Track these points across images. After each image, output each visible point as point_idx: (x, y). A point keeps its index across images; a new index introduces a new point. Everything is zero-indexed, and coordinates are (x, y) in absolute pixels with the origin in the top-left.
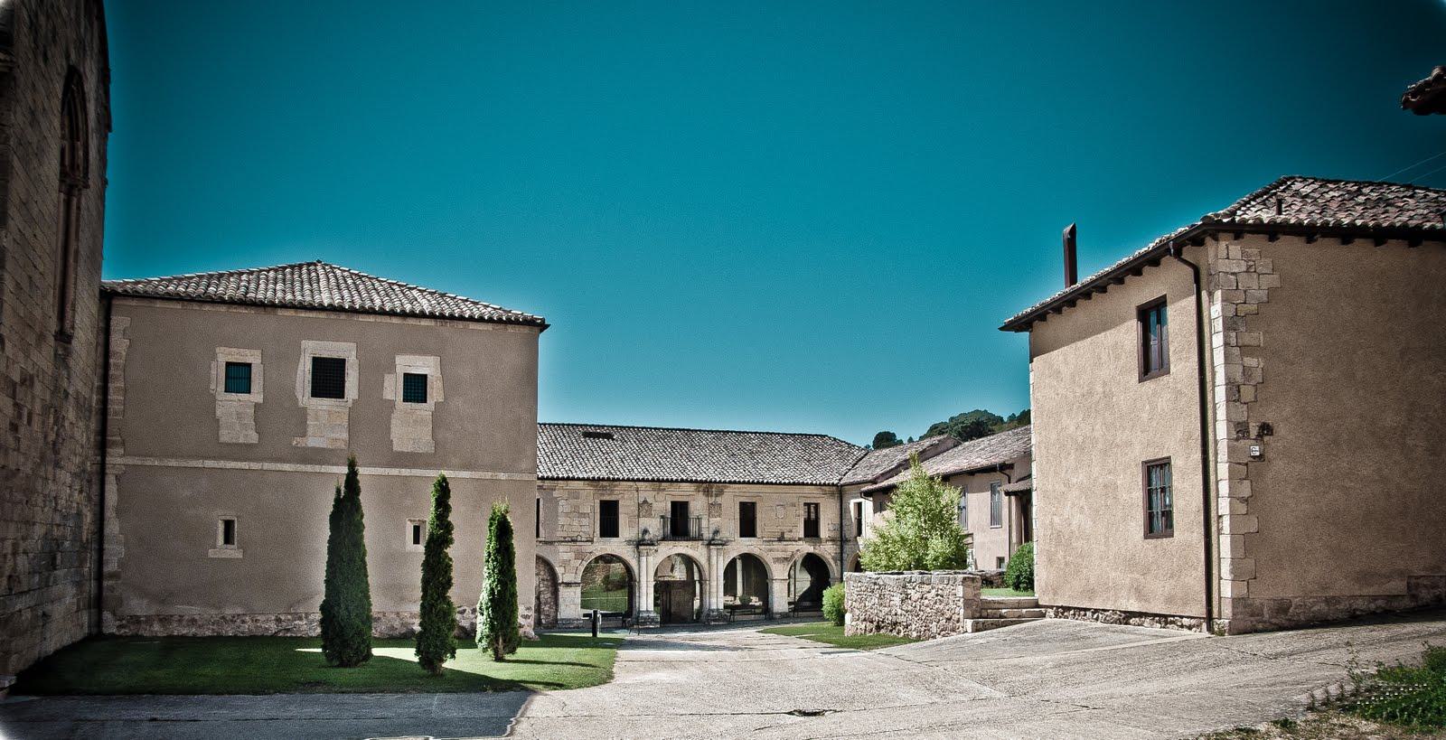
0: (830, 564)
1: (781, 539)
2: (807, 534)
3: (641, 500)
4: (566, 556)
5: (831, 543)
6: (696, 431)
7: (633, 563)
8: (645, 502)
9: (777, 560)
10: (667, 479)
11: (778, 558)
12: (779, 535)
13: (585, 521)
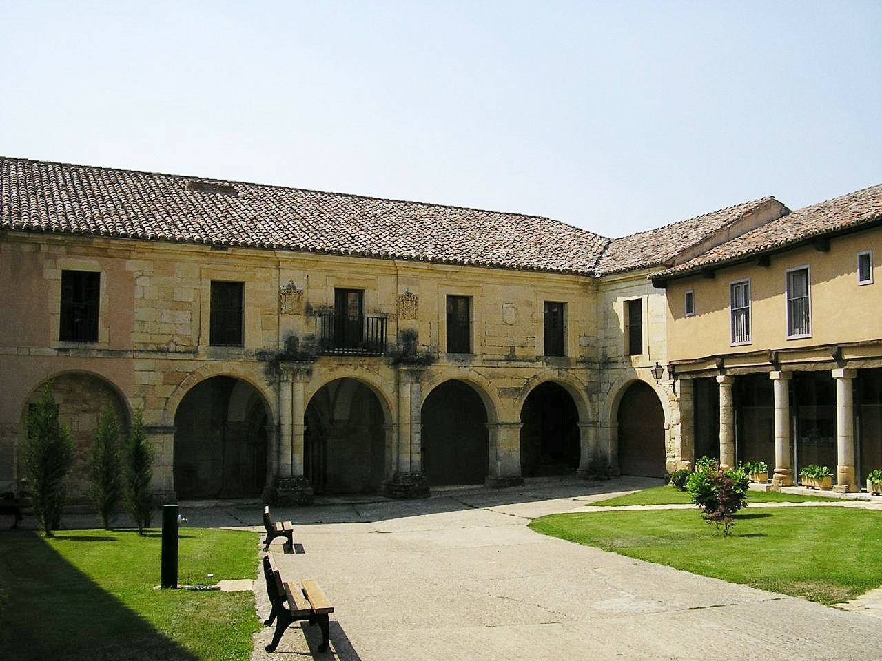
0: (581, 399)
1: (510, 358)
2: (548, 351)
3: (284, 284)
4: (145, 379)
5: (582, 366)
6: (366, 198)
7: (269, 392)
8: (291, 287)
9: (505, 392)
10: (322, 250)
11: (590, 401)
12: (507, 351)
13: (183, 316)
